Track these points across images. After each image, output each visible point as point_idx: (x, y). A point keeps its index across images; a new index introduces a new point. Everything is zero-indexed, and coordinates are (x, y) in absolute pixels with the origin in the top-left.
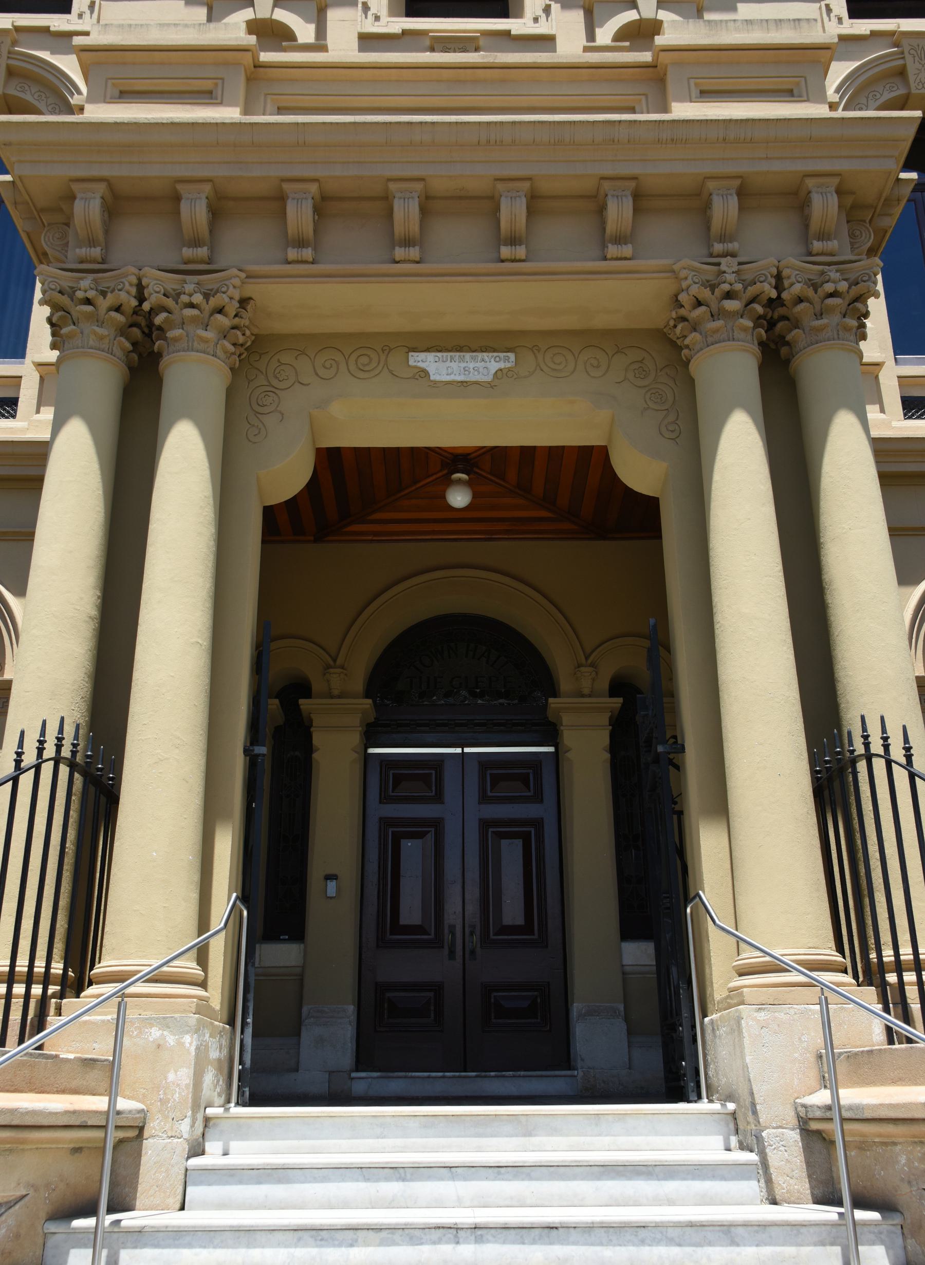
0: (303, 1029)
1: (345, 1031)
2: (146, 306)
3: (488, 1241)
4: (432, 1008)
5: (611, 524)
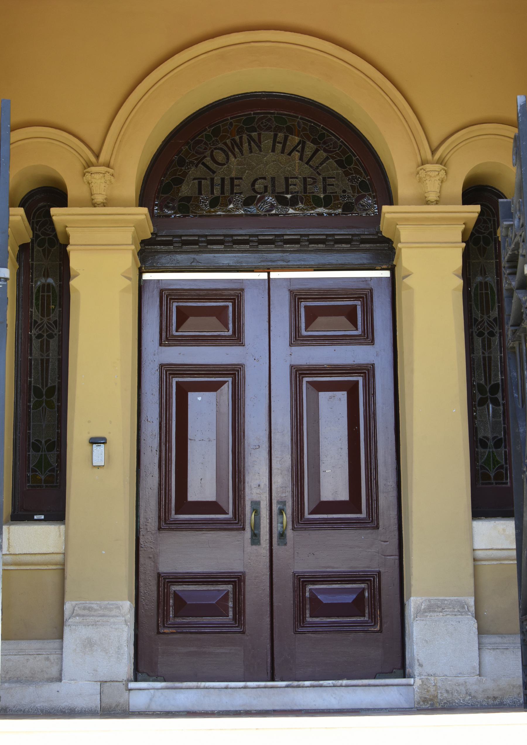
1: (120, 633)
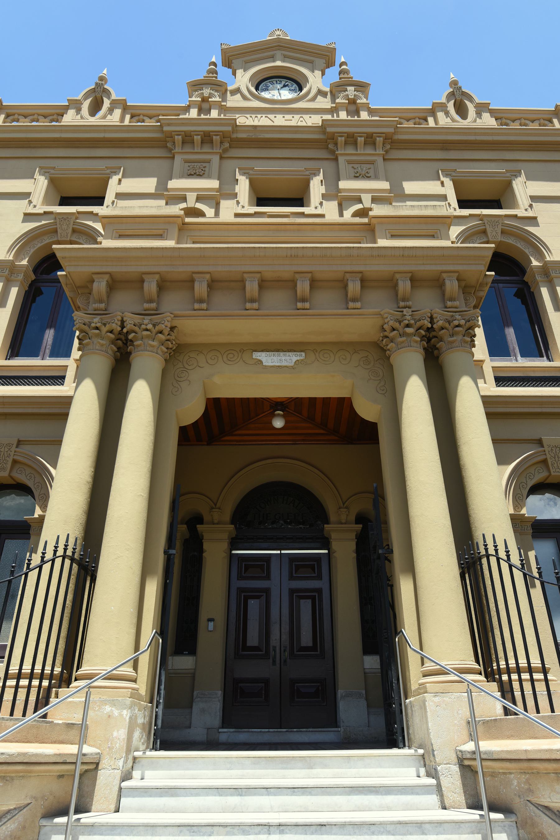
0: (194, 704)
1: (216, 706)
2: (125, 330)
3: (287, 833)
4: (263, 692)
5: (355, 437)
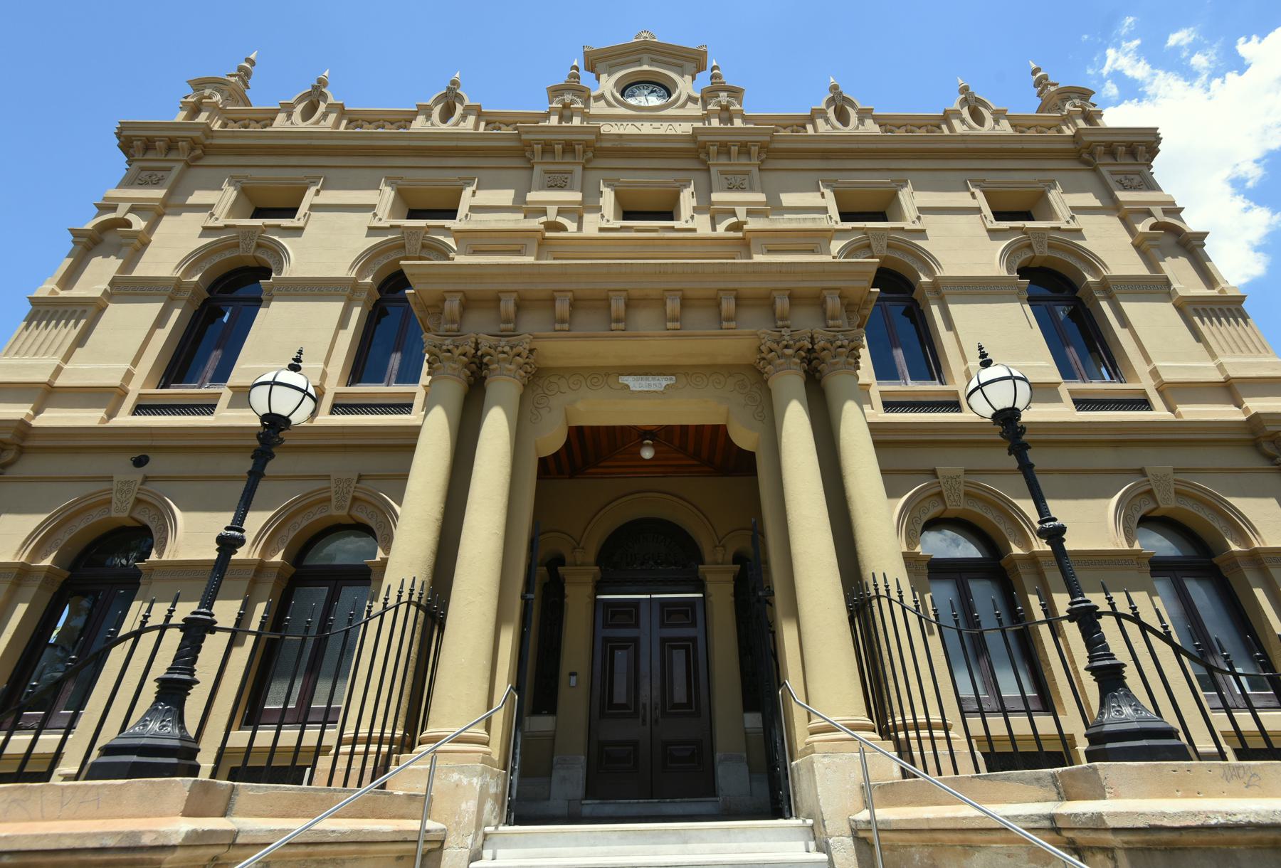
1: (577, 772)
2: (479, 353)
5: (728, 467)
